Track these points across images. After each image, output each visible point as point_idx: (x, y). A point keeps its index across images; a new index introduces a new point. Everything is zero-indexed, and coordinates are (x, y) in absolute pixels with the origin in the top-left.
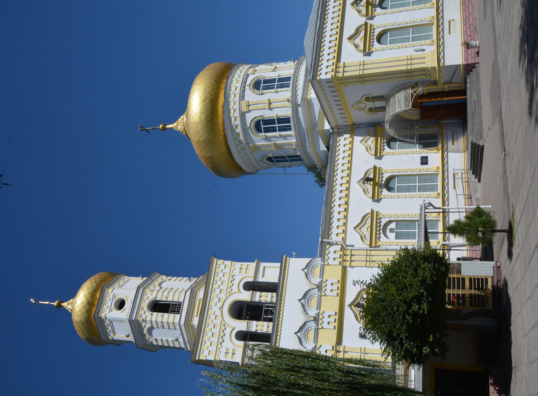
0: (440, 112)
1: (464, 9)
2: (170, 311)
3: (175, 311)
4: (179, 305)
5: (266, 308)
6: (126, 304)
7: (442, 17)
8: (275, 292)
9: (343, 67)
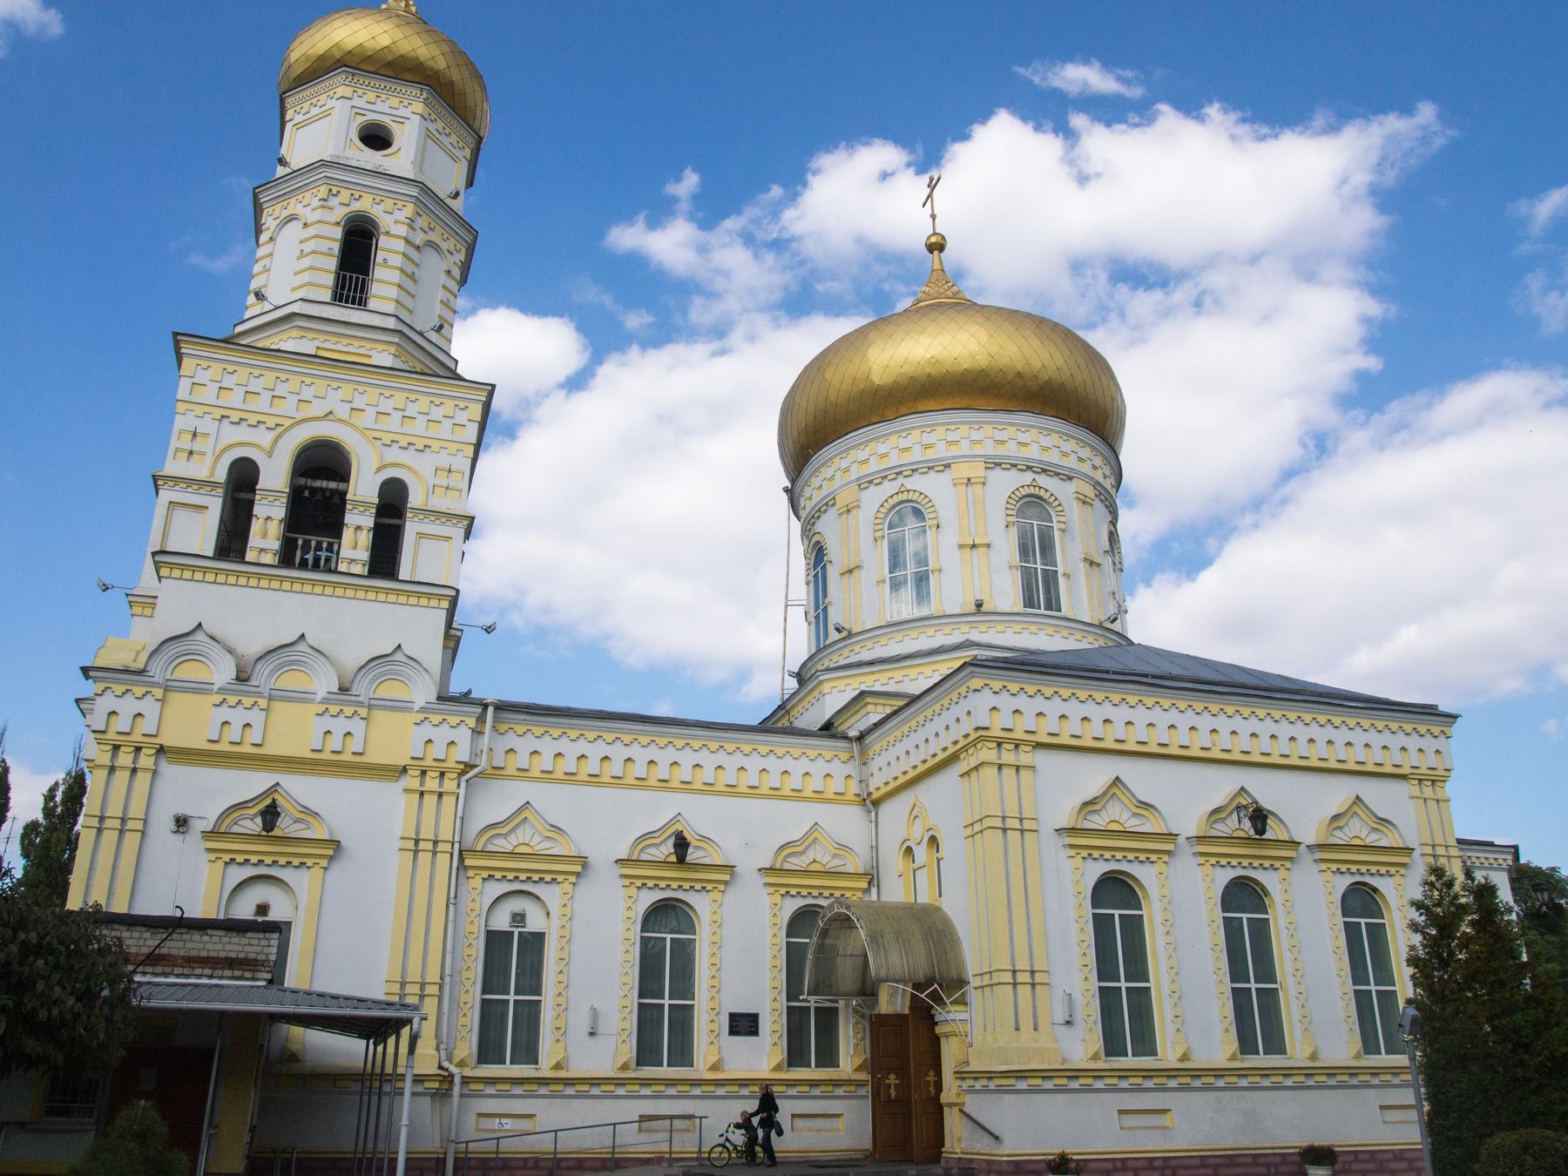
0: (892, 1076)
1: (1211, 1161)
2: (344, 276)
3: (343, 288)
4: (361, 298)
5: (300, 542)
6: (376, 152)
7: (1183, 1088)
8: (370, 572)
9: (1436, 797)
